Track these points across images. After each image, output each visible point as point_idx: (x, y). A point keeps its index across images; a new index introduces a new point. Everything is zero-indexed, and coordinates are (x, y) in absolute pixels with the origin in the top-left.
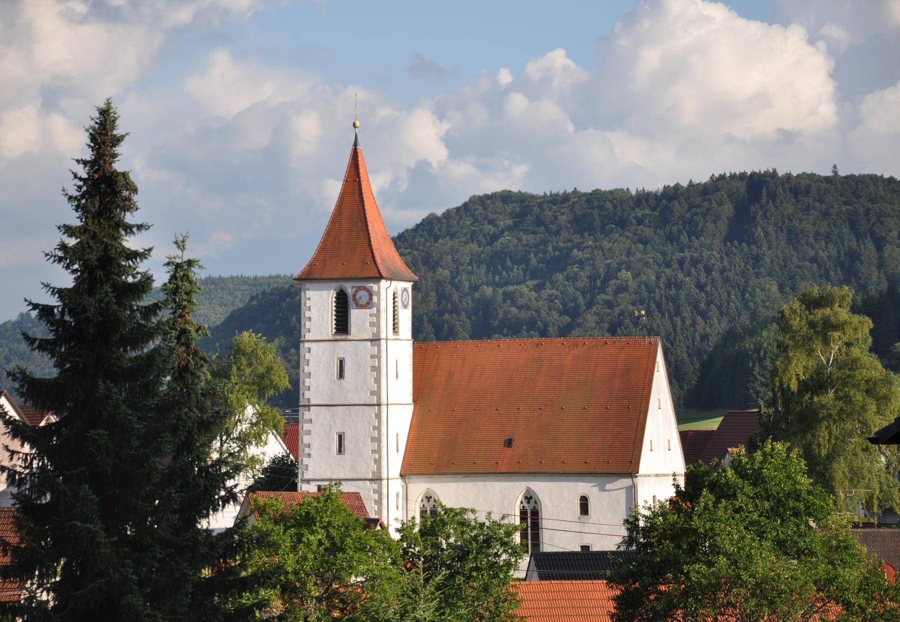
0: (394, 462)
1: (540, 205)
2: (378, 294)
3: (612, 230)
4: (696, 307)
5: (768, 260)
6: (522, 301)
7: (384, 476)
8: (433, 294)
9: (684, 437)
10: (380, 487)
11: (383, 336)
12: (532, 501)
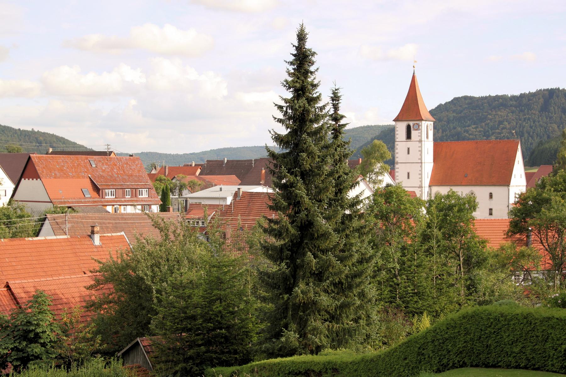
0: (426, 181)
1: (477, 100)
2: (421, 125)
3: (501, 109)
4: (529, 134)
5: (554, 118)
6: (470, 132)
7: (423, 186)
8: (441, 130)
9: (527, 175)
10: (422, 189)
11: (423, 140)
12: (473, 194)
